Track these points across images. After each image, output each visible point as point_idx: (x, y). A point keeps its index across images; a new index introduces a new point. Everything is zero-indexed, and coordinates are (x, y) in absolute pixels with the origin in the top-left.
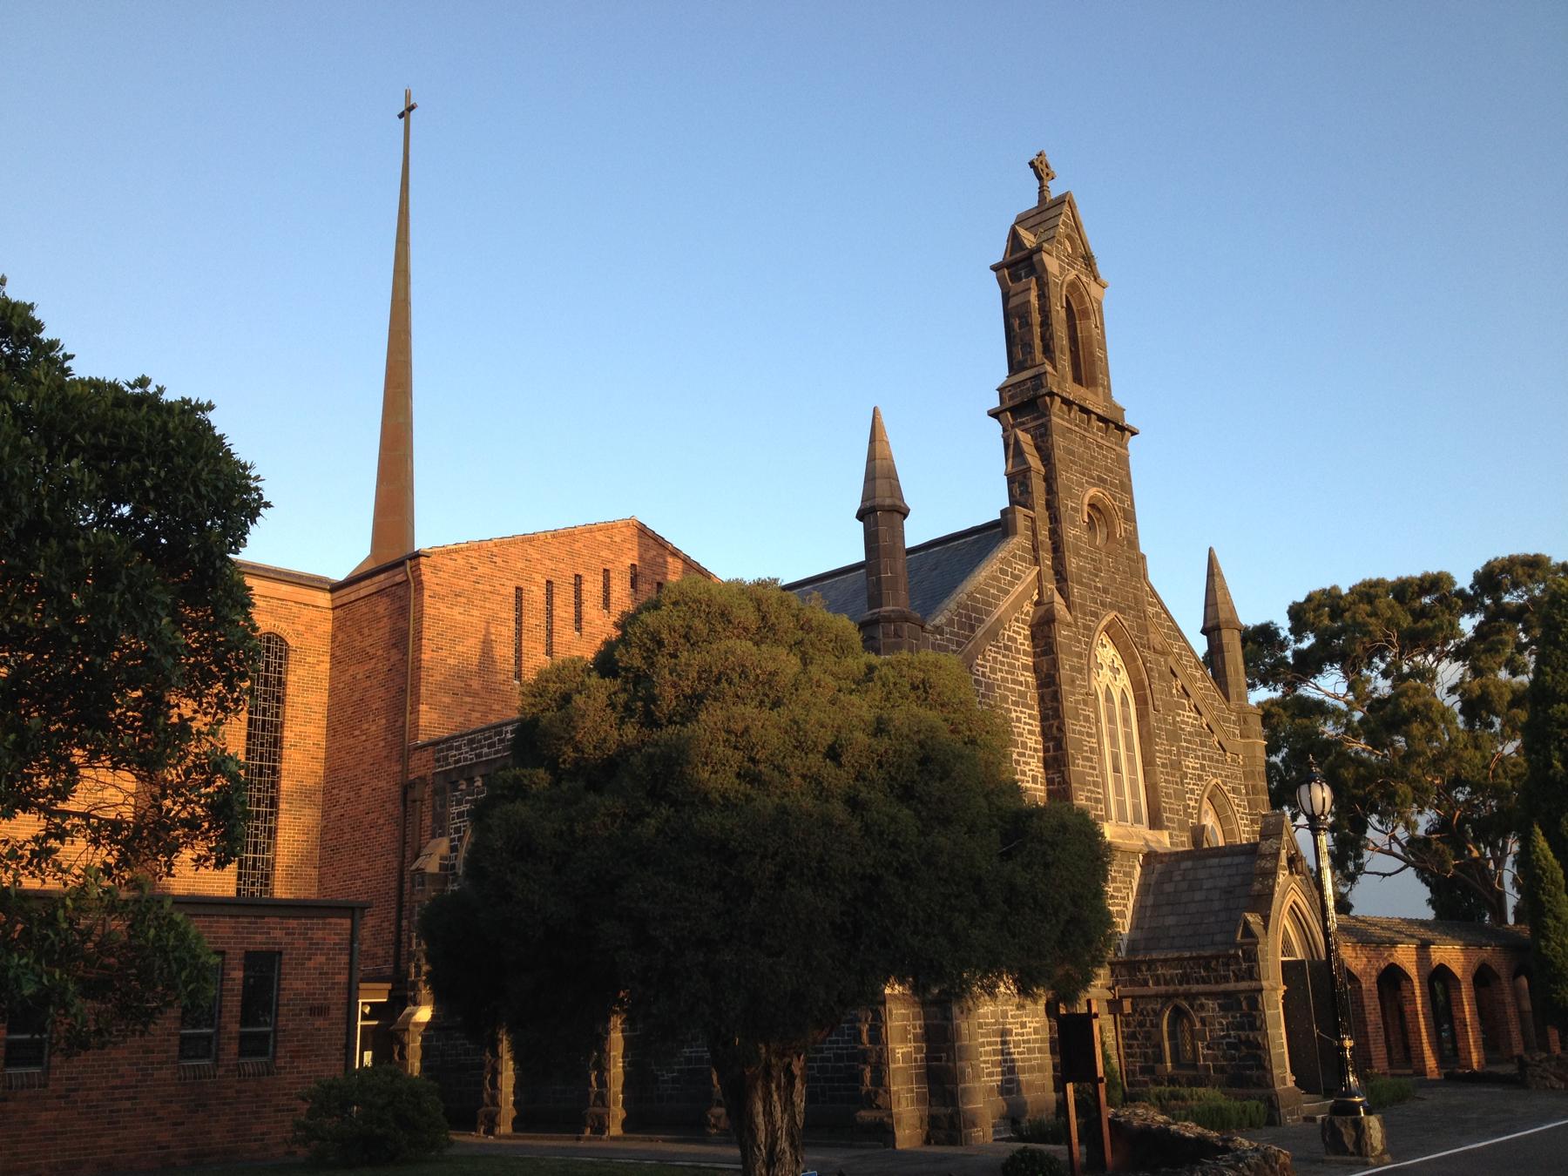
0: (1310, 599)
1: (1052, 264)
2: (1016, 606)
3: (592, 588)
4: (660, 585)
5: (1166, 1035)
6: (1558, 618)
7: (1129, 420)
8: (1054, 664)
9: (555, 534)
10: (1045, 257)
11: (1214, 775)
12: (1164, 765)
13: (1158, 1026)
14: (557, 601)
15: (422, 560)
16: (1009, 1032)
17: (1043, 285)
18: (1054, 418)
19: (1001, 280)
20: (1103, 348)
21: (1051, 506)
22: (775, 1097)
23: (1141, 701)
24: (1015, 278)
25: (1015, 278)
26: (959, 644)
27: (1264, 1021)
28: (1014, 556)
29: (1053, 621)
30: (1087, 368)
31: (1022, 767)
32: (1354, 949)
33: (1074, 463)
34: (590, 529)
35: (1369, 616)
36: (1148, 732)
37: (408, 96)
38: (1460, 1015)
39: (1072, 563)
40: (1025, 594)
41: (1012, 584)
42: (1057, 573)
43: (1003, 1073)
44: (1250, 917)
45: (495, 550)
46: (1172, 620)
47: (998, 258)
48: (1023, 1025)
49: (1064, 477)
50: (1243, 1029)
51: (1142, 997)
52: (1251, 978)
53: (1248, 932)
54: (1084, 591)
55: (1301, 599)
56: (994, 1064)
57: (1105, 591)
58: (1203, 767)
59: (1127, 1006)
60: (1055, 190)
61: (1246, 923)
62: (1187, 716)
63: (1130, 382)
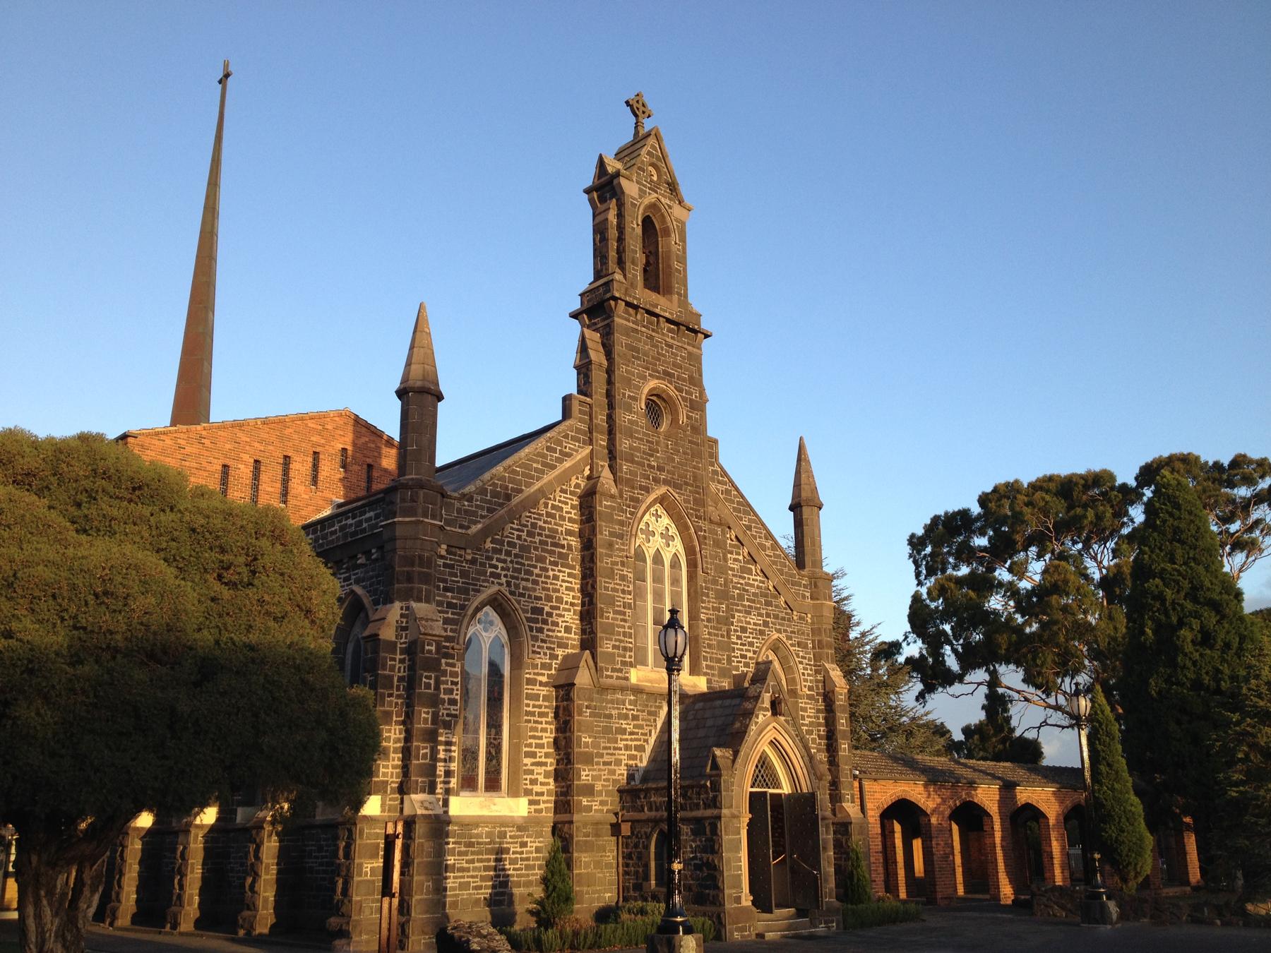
0: (996, 490)
1: (630, 188)
2: (564, 478)
3: (301, 467)
4: (370, 466)
5: (652, 856)
6: (1157, 505)
7: (705, 325)
8: (593, 531)
9: (266, 422)
10: (623, 182)
11: (779, 631)
12: (709, 620)
13: (647, 847)
14: (263, 477)
15: (130, 440)
16: (507, 851)
17: (620, 205)
18: (616, 319)
19: (591, 201)
20: (683, 260)
21: (609, 395)
22: (45, 902)
23: (692, 565)
24: (602, 200)
25: (602, 200)
26: (489, 510)
27: (721, 845)
28: (566, 436)
29: (595, 493)
30: (660, 272)
31: (555, 618)
32: (926, 786)
33: (638, 358)
34: (302, 418)
35: (1027, 505)
36: (696, 592)
37: (226, 65)
38: (1047, 849)
39: (624, 444)
40: (576, 469)
41: (560, 461)
42: (610, 452)
43: (494, 887)
44: (718, 752)
45: (204, 433)
46: (742, 497)
47: (589, 182)
48: (524, 845)
49: (621, 370)
50: (706, 852)
51: (638, 821)
52: (716, 807)
53: (715, 766)
54: (633, 467)
55: (989, 489)
56: (483, 878)
57: (660, 469)
58: (766, 624)
59: (626, 829)
60: (648, 125)
61: (714, 757)
62: (755, 579)
63: (706, 286)
